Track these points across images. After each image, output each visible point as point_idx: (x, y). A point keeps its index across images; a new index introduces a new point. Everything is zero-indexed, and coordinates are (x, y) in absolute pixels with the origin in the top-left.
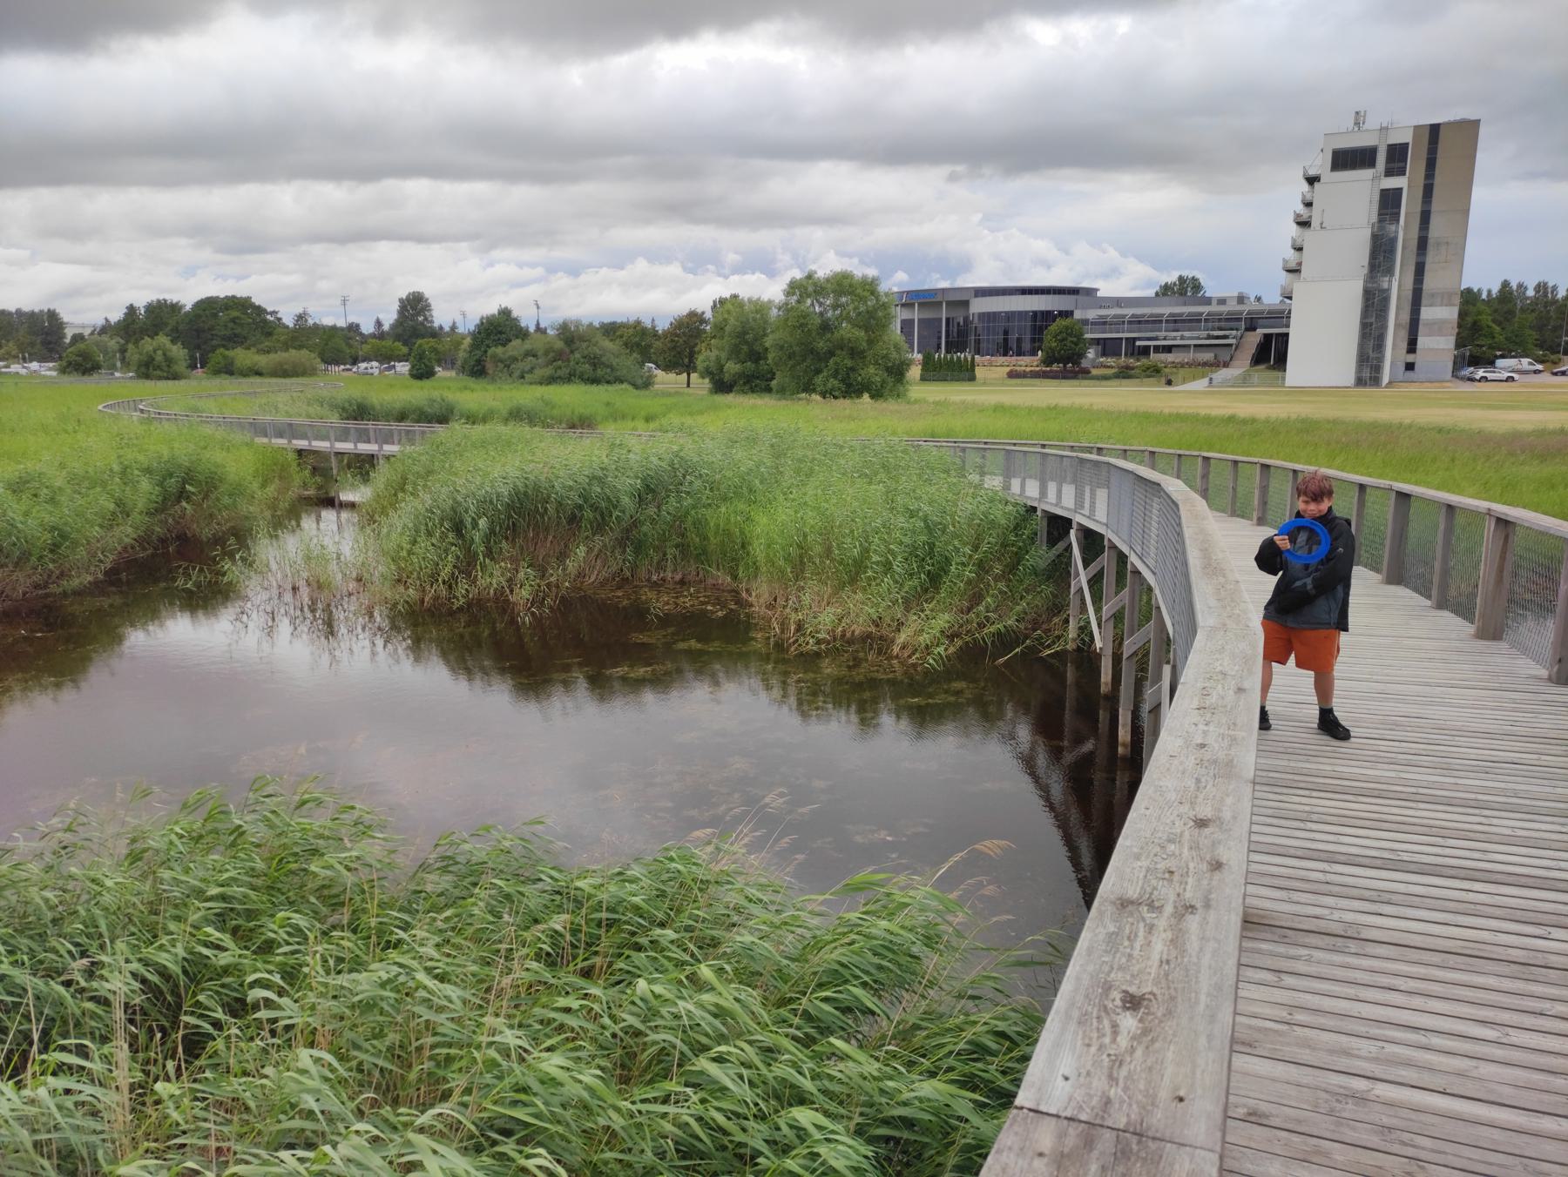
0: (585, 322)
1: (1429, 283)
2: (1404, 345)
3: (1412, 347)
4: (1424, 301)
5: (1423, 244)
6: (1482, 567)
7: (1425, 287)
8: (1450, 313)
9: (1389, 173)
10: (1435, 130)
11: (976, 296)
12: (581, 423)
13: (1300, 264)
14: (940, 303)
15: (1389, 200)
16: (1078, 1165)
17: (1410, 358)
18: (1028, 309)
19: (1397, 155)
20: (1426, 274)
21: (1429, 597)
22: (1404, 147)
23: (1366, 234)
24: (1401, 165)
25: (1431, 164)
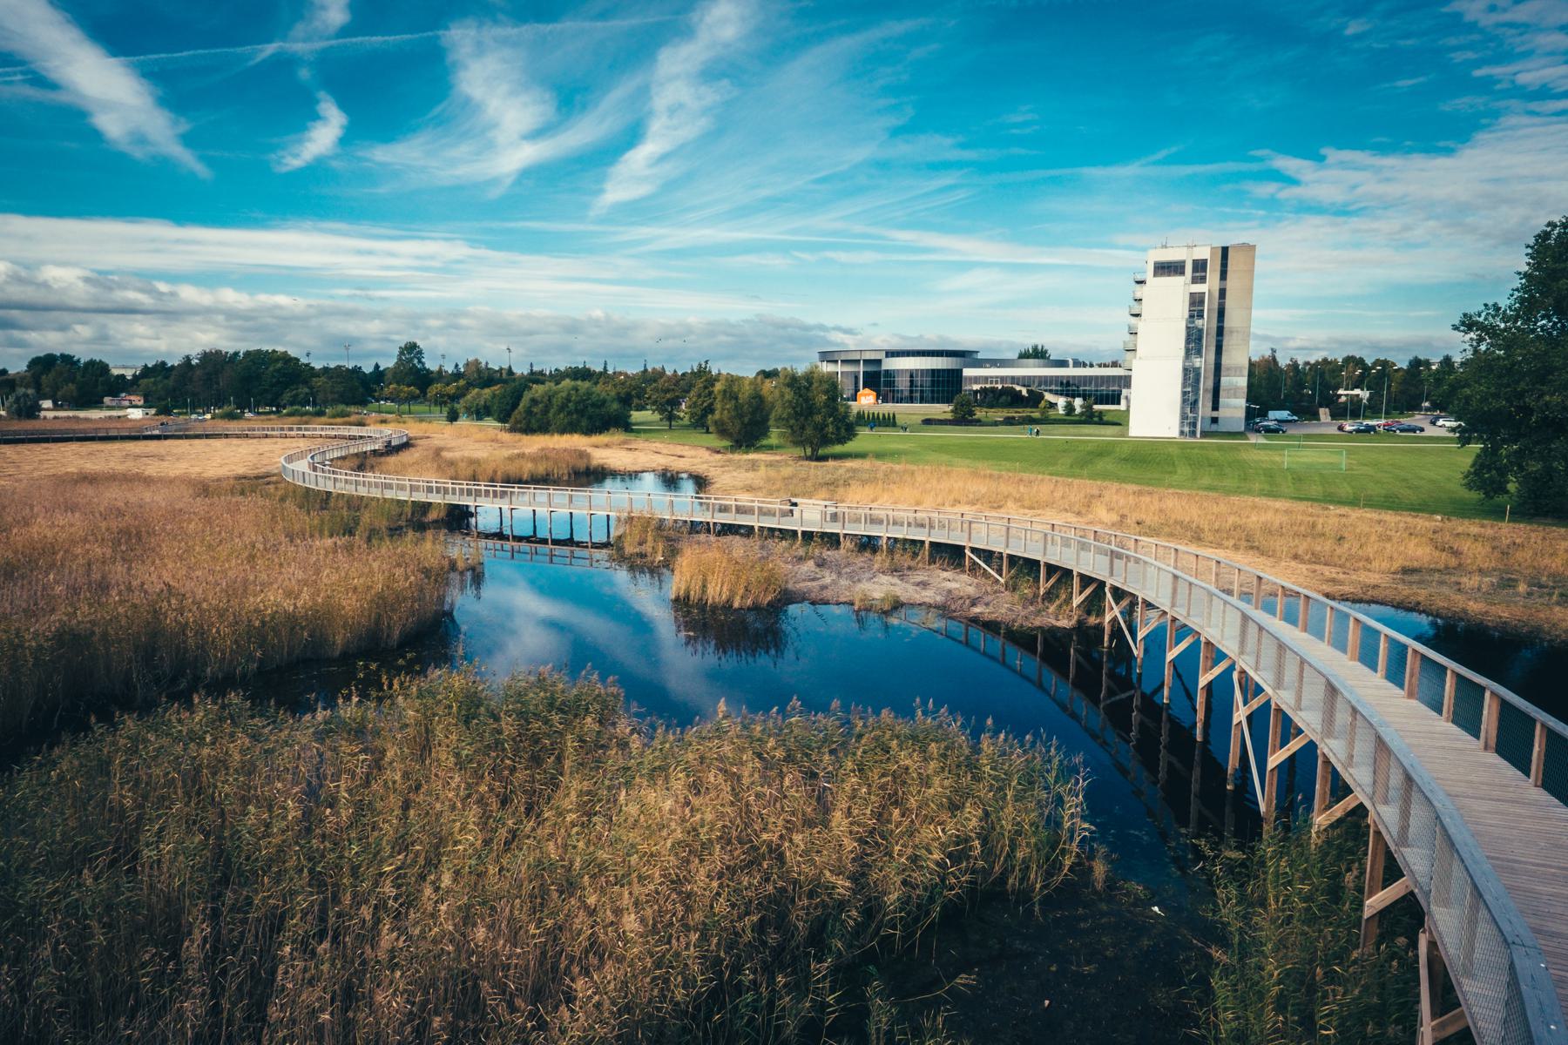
0: (612, 467)
1: (1225, 360)
2: (1210, 404)
3: (1215, 407)
4: (1223, 373)
5: (1220, 331)
6: (185, 54)
7: (1223, 362)
8: (1242, 382)
9: (1195, 281)
10: (1225, 251)
11: (887, 356)
12: (591, 476)
13: (1135, 345)
14: (858, 361)
15: (1196, 301)
16: (773, 652)
17: (1215, 414)
18: (918, 368)
19: (1200, 266)
20: (1224, 353)
21: (1401, 686)
22: (1205, 261)
23: (1182, 326)
24: (1203, 274)
25: (1223, 275)
